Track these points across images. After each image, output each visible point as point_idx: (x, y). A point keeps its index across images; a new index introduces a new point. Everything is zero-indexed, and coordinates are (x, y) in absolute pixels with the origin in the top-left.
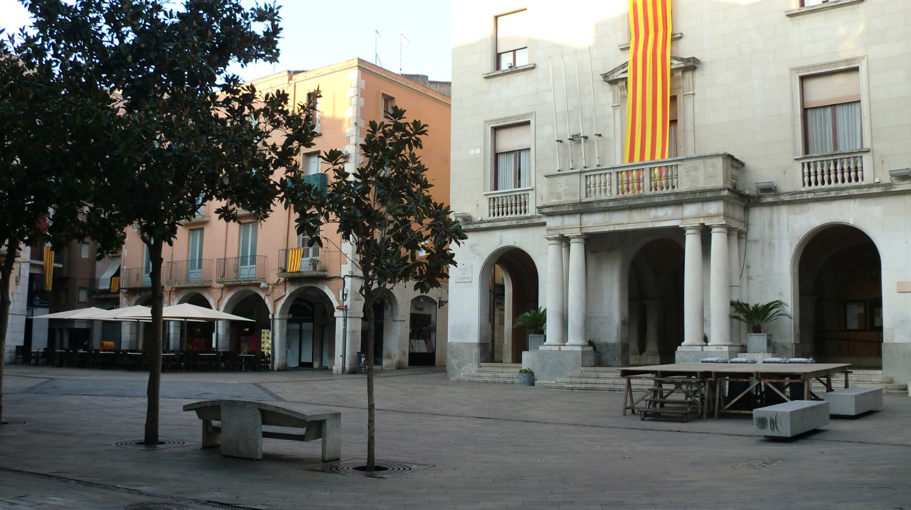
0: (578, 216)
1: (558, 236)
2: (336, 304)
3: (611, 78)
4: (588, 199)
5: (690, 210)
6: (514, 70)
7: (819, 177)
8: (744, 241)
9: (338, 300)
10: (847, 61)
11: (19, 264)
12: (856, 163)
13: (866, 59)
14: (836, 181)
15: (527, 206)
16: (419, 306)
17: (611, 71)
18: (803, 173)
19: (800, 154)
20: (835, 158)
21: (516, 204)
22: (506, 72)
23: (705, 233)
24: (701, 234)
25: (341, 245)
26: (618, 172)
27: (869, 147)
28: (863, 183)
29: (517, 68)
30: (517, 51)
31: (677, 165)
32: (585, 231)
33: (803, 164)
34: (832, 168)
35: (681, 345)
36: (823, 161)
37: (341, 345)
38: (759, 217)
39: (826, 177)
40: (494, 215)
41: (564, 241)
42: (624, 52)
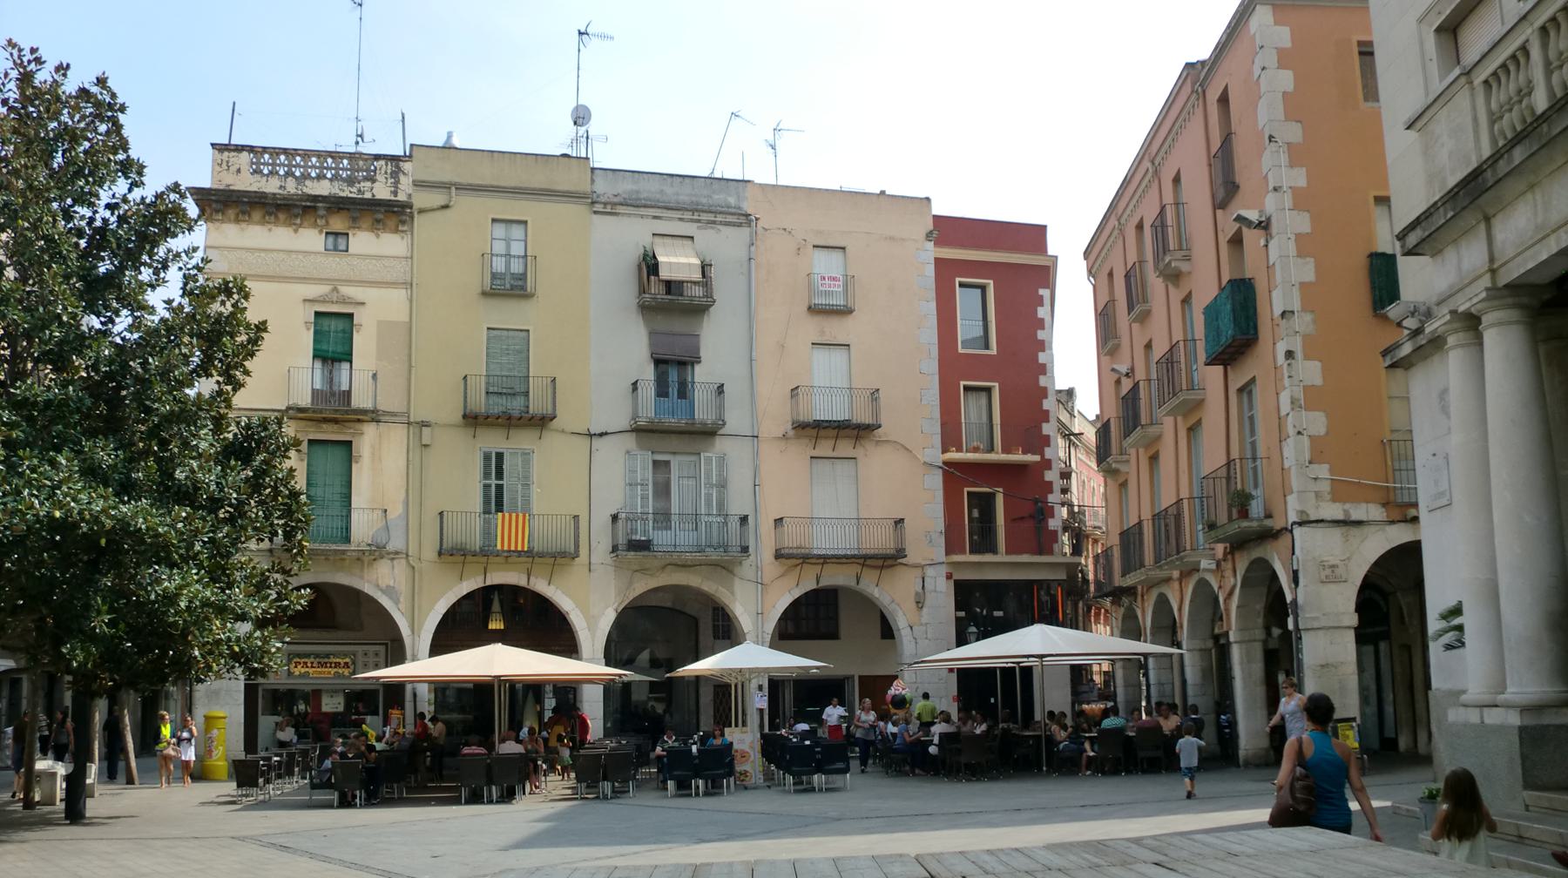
11: (918, 572)
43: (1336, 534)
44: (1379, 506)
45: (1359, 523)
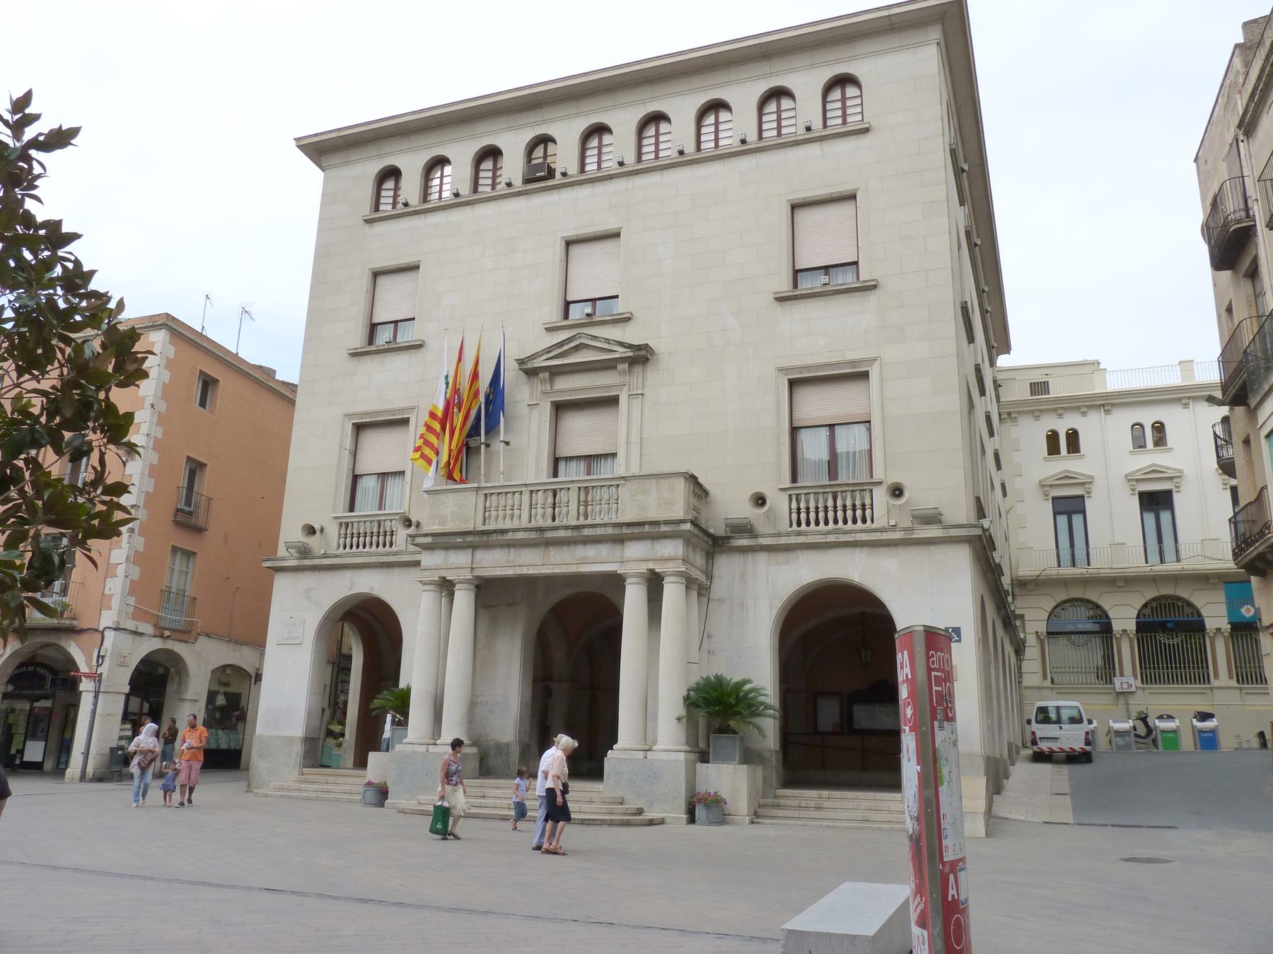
0: (469, 551)
1: (437, 579)
2: (83, 668)
3: (529, 365)
4: (486, 528)
5: (635, 550)
6: (394, 348)
7: (812, 515)
8: (705, 599)
9: (88, 664)
10: (853, 363)
12: (862, 498)
13: (878, 361)
14: (836, 522)
15: (394, 537)
16: (224, 680)
17: (531, 356)
18: (790, 509)
19: (787, 483)
20: (834, 490)
21: (379, 533)
22: (381, 348)
23: (654, 583)
24: (647, 584)
25: (105, 581)
26: (532, 492)
27: (882, 478)
28: (874, 526)
29: (398, 343)
30: (399, 323)
31: (618, 485)
32: (478, 573)
33: (790, 496)
34: (830, 503)
35: (612, 749)
36: (818, 493)
37: (85, 736)
38: (726, 566)
39: (821, 515)
40: (345, 548)
41: (446, 587)
42: (549, 333)
43: (130, 637)
44: (151, 626)
45: (142, 634)
